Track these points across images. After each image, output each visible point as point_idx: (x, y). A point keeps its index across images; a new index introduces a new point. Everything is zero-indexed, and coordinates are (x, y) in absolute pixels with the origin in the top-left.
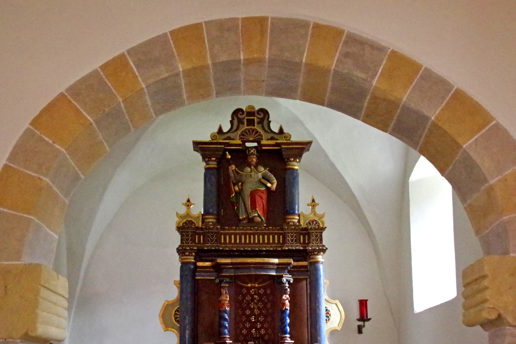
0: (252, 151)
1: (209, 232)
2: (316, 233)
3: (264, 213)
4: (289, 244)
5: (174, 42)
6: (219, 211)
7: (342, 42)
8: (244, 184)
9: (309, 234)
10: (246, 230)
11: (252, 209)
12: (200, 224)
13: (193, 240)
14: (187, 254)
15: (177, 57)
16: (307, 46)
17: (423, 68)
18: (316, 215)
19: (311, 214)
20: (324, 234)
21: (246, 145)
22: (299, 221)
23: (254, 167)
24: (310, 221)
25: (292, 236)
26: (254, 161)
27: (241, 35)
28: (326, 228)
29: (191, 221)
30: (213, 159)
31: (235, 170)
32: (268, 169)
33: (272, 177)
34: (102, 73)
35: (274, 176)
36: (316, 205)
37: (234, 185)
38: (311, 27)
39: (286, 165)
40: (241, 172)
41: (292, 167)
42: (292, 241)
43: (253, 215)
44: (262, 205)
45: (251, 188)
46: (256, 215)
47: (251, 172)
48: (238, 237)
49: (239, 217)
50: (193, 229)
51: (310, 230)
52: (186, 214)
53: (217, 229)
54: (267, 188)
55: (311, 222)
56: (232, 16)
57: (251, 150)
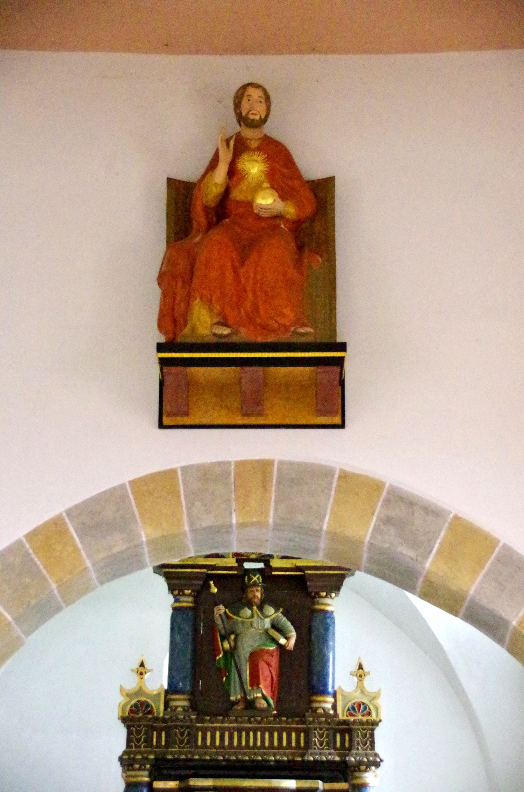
0: (255, 579)
1: (176, 727)
2: (364, 730)
3: (273, 691)
4: (315, 749)
5: (135, 499)
6: (194, 685)
7: (381, 500)
8: (240, 638)
9: (350, 731)
10: (241, 723)
11: (252, 685)
12: (162, 708)
13: (148, 741)
14: (137, 766)
15: (139, 520)
16: (330, 506)
17: (501, 545)
18: (366, 694)
19: (356, 690)
20: (378, 732)
21: (244, 567)
22: (334, 707)
23: (257, 608)
24: (354, 704)
25: (321, 736)
26: (258, 598)
27: (233, 487)
28: (380, 721)
29: (146, 702)
30: (187, 592)
31: (225, 613)
32: (281, 610)
33: (288, 627)
34: (27, 546)
35: (292, 624)
36: (364, 674)
37: (224, 638)
38: (336, 476)
39: (314, 603)
40: (234, 617)
41: (323, 607)
42: (321, 744)
43: (254, 695)
44: (269, 679)
45: (252, 646)
46: (259, 695)
47: (252, 617)
48: (227, 734)
49: (229, 696)
50: (150, 720)
51: (353, 725)
52: (136, 689)
53: (191, 720)
54: (281, 647)
55: (355, 706)
56: (220, 459)
57: (253, 577)
